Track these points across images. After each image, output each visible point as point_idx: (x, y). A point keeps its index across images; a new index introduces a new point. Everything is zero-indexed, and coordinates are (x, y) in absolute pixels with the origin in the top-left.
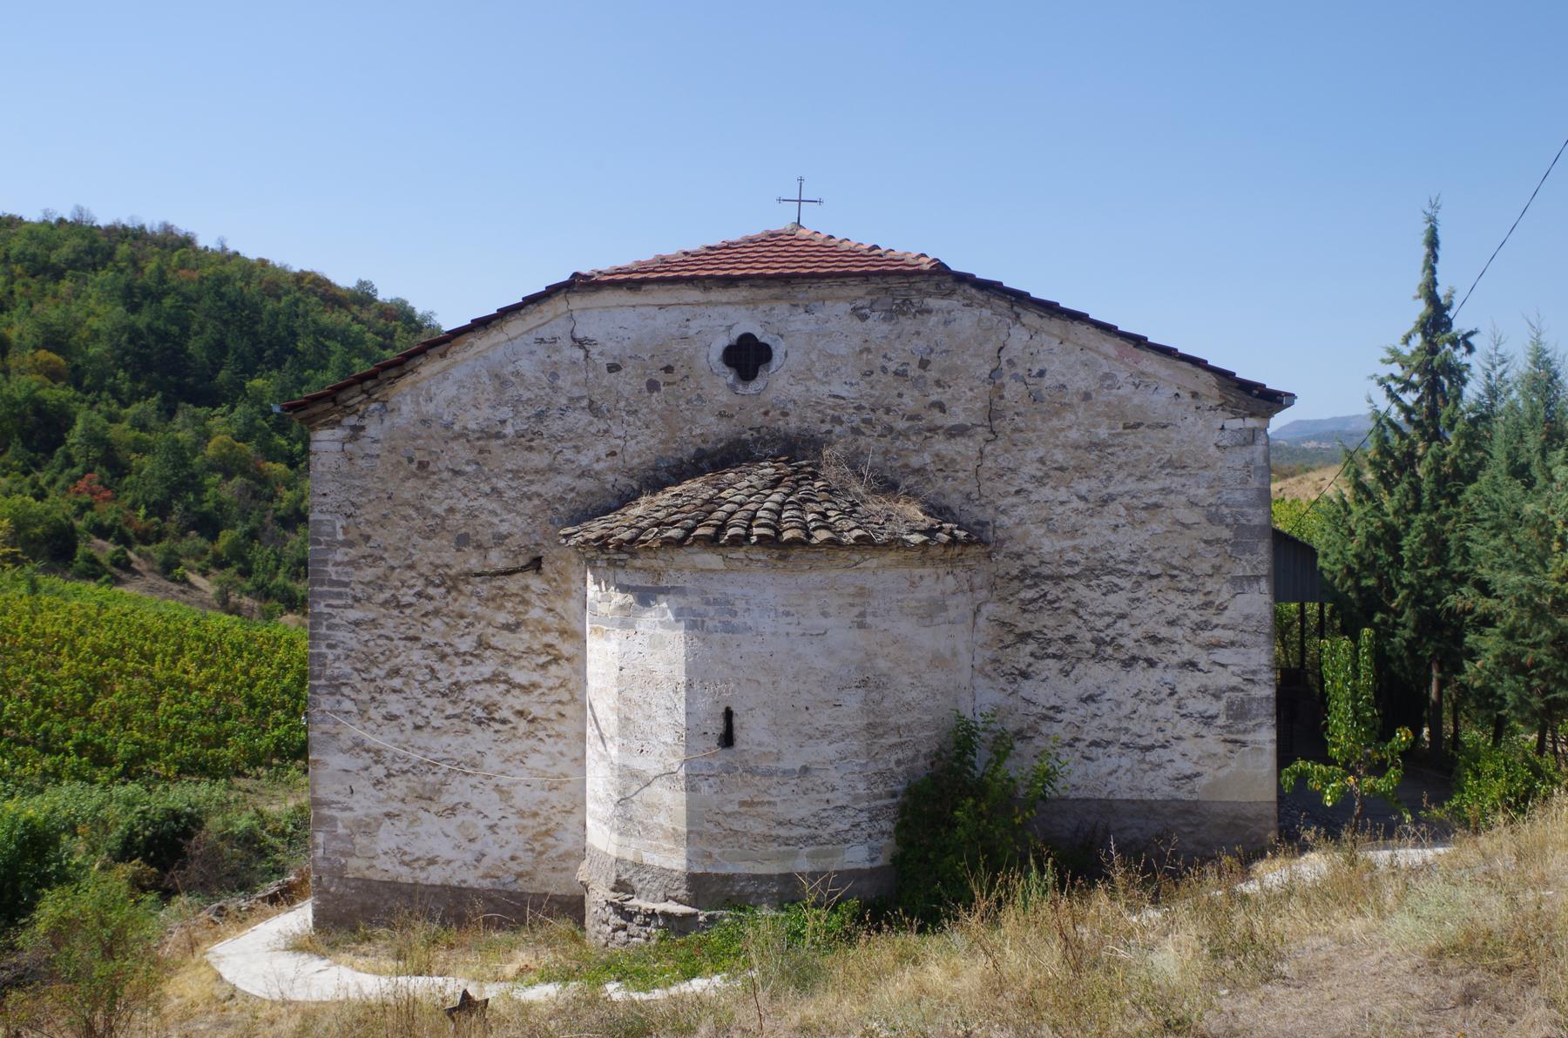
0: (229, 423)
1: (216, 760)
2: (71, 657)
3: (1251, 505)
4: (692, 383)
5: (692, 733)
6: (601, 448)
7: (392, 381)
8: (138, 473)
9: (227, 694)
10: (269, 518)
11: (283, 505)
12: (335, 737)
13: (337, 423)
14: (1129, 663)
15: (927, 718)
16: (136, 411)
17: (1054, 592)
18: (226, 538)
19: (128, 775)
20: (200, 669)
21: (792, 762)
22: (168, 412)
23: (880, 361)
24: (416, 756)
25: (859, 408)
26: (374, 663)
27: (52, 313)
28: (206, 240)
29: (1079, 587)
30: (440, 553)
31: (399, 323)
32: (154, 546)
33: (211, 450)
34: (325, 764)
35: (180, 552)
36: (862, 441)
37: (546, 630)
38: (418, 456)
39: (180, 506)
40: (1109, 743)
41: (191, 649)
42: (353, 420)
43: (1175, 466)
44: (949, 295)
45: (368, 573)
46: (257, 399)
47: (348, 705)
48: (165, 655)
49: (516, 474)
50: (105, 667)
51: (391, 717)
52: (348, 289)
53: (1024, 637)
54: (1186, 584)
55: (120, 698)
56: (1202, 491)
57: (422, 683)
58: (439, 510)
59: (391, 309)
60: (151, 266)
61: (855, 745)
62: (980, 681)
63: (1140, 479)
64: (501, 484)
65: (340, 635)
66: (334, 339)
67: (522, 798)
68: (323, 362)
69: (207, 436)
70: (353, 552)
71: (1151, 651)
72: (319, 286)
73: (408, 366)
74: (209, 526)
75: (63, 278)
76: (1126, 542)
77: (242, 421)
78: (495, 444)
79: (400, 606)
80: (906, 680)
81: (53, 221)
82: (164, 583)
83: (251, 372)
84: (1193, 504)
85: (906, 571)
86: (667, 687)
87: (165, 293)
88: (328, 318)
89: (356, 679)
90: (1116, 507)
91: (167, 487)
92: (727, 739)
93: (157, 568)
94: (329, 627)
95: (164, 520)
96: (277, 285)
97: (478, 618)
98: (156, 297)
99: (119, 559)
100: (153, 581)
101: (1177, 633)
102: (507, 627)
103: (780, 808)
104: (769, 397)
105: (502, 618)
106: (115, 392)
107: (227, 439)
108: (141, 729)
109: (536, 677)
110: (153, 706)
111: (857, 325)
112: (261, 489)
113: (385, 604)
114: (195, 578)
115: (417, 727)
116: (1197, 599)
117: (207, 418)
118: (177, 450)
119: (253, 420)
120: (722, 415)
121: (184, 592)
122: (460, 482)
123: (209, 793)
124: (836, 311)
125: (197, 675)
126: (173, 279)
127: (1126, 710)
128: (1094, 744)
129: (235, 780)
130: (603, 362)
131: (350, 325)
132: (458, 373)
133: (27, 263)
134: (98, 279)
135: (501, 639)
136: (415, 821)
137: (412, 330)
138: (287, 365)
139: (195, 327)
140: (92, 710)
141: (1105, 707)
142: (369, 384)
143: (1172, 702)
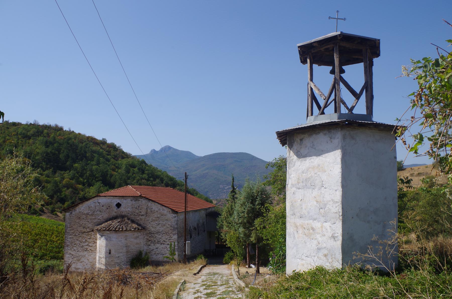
0: (69, 175)
1: (58, 256)
2: (31, 236)
3: (175, 225)
4: (112, 209)
5: (106, 252)
6: (101, 216)
7: (76, 207)
8: (47, 188)
9: (61, 243)
10: (77, 199)
11: (81, 195)
12: (67, 252)
13: (69, 212)
14: (161, 244)
15: (135, 251)
16: (47, 173)
17: (153, 235)
18: (66, 204)
19: (41, 259)
20: (56, 238)
21: (117, 256)
22: (54, 172)
23: (134, 206)
24: (77, 255)
25: (131, 212)
26: (73, 243)
27: (28, 149)
28: (66, 128)
29: (156, 234)
30: (81, 229)
31: (112, 149)
32: (50, 206)
33: (64, 182)
34: (66, 256)
35: (56, 207)
36: (132, 216)
37: (94, 239)
38: (79, 216)
39: (56, 196)
40: (159, 254)
41: (55, 233)
42: (71, 212)
43: (167, 220)
44: (142, 199)
45: (72, 231)
46: (76, 169)
47: (69, 248)
48: (50, 235)
49: (91, 219)
50: (37, 237)
51: (74, 250)
52: (100, 140)
53: (150, 241)
54: (168, 234)
55: (40, 244)
56: (170, 223)
57: (78, 246)
58: (81, 223)
59: (110, 145)
60: (52, 136)
61: (125, 254)
62: (144, 246)
63: (163, 221)
64: (89, 220)
65: (68, 239)
66: (96, 153)
67: (90, 260)
68: (93, 159)
69: (63, 178)
70: (70, 229)
71: (164, 242)
72: (93, 140)
73: (78, 205)
74: (62, 201)
75: (31, 139)
76: (161, 229)
77: (72, 174)
78: (88, 215)
79: (76, 236)
80: (132, 246)
81: (29, 124)
82: (51, 215)
83: (75, 162)
84: (169, 225)
85: (133, 233)
86: (104, 247)
87: (55, 143)
88: (94, 148)
89: (70, 245)
90: (160, 225)
91: (53, 192)
92: (110, 253)
93: (50, 211)
94: (67, 238)
95: (52, 199)
96: (82, 140)
97: (86, 237)
98: (52, 143)
99: (41, 210)
100: (49, 215)
101: (167, 240)
102: (89, 239)
103: (115, 261)
104: (121, 210)
105: (88, 237)
106: (42, 168)
107: (68, 179)
108: (44, 250)
109: (92, 245)
110: (46, 245)
111: (131, 202)
112: (76, 191)
113: (74, 235)
114: (59, 214)
115: (78, 251)
116: (169, 236)
117: (64, 174)
118: (56, 182)
119: (75, 174)
120: (115, 212)
121: (56, 217)
122: (84, 220)
123: (56, 263)
124: (129, 200)
125: (56, 239)
126: (58, 138)
127: (161, 250)
128: (157, 254)
129: (62, 260)
130: (102, 205)
131: (100, 150)
132: (84, 206)
133: (22, 135)
134: (39, 139)
135: (88, 240)
136: (77, 263)
137: (116, 150)
138: (84, 160)
139: (62, 151)
140: (34, 246)
141: (159, 249)
142: (73, 207)
143: (166, 249)
